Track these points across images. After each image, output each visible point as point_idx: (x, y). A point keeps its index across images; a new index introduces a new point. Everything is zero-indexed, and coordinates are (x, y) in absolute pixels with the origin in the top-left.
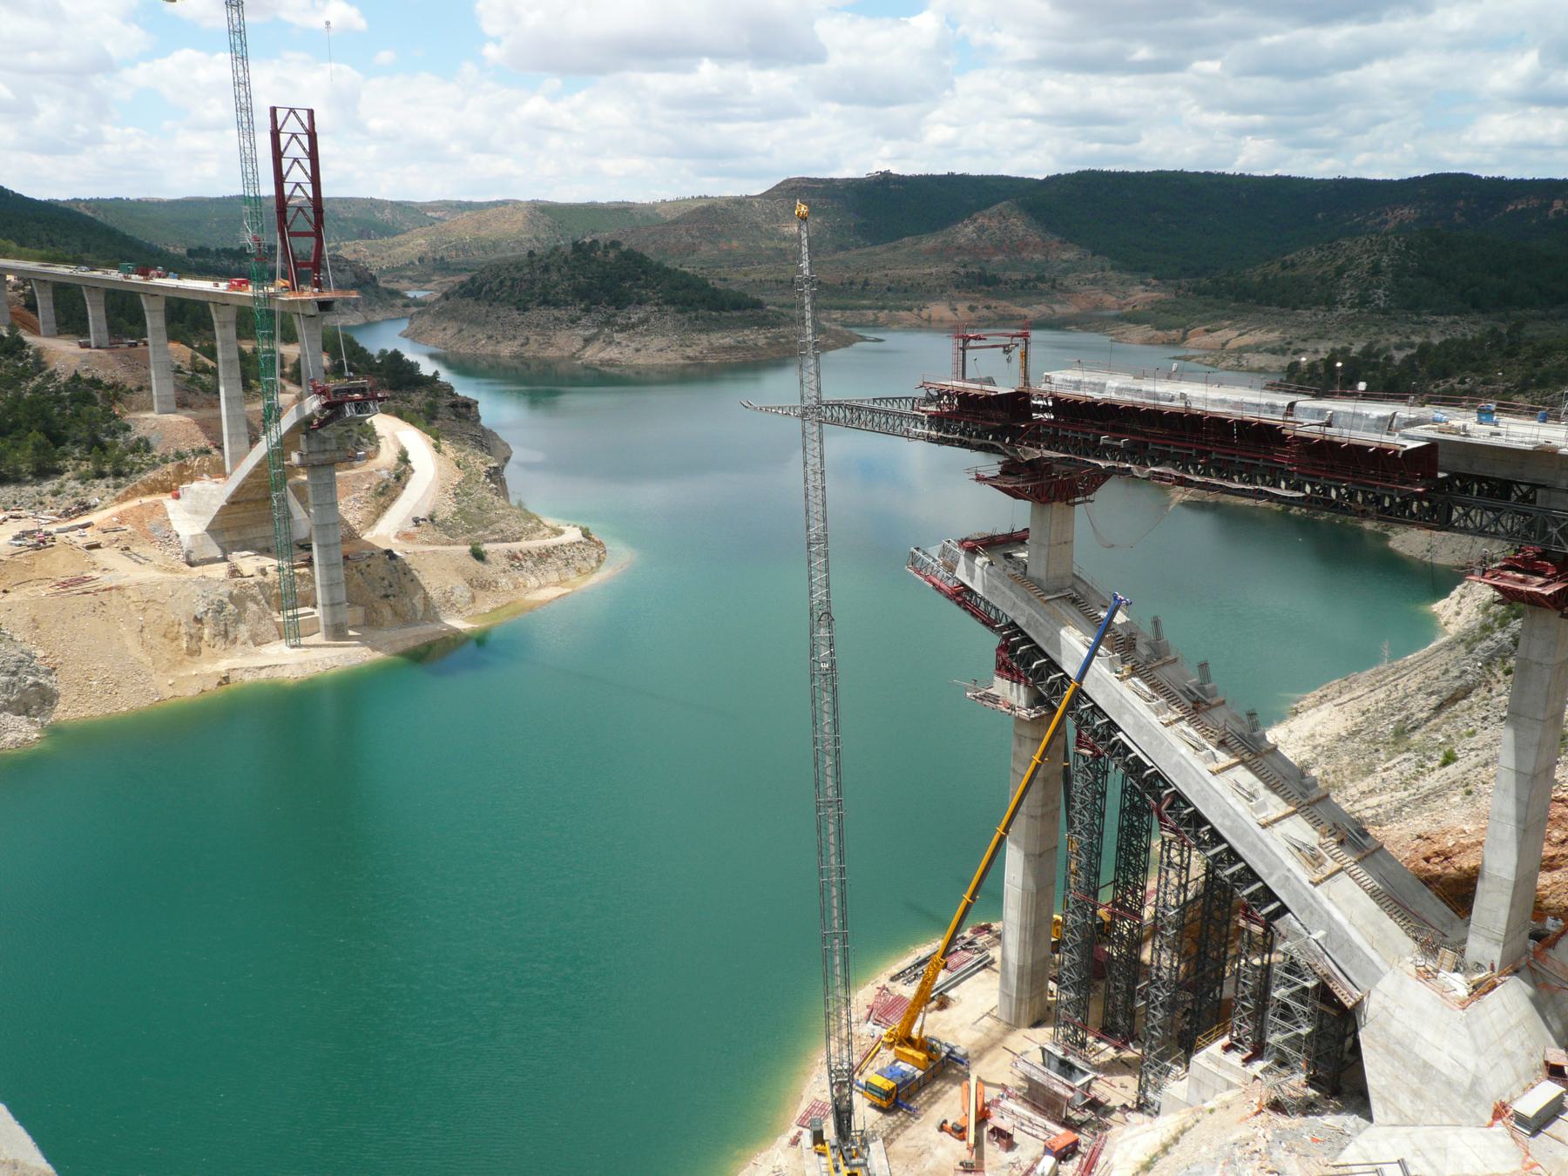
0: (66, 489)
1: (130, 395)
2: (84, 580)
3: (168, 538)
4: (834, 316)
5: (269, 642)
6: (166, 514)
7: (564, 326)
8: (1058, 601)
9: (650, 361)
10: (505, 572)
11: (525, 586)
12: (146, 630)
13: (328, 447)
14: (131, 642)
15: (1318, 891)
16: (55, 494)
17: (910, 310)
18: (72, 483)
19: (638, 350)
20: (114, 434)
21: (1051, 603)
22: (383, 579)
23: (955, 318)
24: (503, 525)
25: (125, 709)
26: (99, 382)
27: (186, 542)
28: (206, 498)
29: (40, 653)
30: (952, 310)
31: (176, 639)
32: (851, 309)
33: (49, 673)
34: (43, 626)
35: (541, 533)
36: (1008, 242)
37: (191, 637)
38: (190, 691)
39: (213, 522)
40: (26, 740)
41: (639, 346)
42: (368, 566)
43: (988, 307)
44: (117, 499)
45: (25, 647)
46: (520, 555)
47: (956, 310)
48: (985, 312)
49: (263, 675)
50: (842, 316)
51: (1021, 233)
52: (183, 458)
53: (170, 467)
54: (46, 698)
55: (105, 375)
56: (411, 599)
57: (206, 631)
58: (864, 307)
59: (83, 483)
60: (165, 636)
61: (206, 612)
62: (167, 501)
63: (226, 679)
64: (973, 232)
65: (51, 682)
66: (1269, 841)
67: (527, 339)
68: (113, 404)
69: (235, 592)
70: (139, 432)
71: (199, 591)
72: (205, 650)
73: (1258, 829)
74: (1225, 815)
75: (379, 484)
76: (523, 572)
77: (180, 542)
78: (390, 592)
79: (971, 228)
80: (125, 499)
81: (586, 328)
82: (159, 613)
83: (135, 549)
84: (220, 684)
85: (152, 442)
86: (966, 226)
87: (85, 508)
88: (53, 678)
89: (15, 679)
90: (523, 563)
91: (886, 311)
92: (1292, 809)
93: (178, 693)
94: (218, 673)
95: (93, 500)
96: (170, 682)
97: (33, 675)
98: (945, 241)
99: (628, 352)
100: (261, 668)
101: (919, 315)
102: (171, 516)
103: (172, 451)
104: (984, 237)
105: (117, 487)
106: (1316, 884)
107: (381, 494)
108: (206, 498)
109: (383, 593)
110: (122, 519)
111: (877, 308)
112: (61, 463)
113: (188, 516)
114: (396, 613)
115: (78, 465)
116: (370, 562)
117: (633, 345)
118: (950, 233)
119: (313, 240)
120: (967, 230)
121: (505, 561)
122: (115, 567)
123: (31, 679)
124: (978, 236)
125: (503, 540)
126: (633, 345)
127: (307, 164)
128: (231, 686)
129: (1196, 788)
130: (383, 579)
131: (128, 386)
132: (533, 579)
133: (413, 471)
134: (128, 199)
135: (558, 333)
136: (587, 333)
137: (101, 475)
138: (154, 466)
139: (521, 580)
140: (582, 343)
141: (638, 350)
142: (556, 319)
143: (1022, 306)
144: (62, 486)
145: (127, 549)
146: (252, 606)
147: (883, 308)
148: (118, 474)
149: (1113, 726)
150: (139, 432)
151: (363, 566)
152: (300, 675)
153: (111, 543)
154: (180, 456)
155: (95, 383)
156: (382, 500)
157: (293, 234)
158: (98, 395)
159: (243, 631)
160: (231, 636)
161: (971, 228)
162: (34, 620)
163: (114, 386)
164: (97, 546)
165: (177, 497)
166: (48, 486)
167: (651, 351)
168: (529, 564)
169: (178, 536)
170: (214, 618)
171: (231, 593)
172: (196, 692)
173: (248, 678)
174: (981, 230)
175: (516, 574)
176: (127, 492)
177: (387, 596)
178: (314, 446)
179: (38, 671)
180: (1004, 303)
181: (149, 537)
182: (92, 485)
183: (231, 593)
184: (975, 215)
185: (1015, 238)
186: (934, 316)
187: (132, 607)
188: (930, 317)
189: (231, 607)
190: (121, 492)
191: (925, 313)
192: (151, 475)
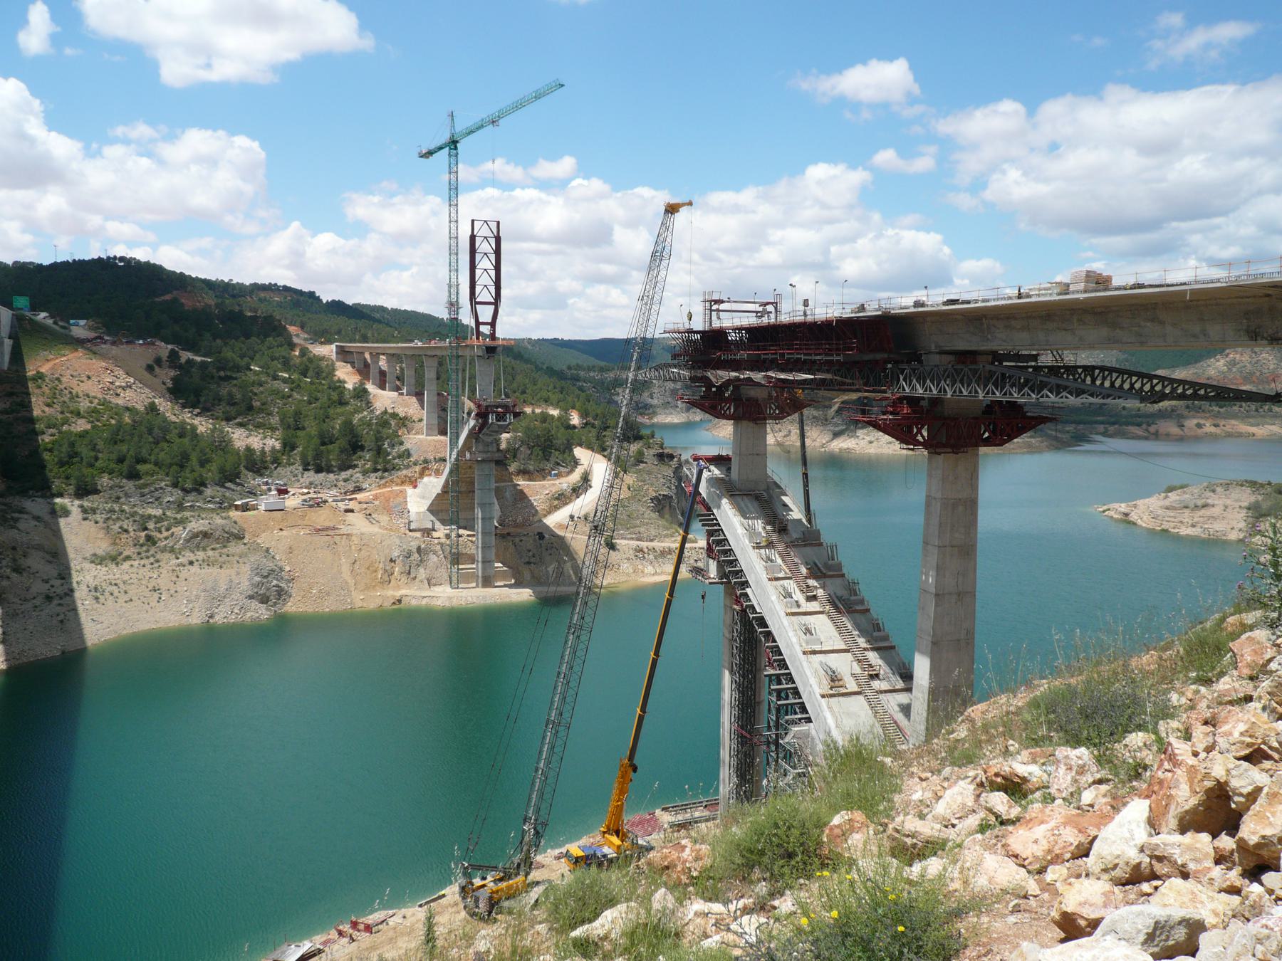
0: (353, 479)
1: (413, 424)
2: (334, 528)
3: (403, 511)
4: (1067, 429)
5: (441, 584)
6: (405, 498)
7: (820, 423)
8: (745, 497)
9: (879, 451)
10: (628, 559)
11: (642, 572)
12: (358, 563)
13: (490, 449)
14: (346, 570)
15: (824, 702)
16: (346, 480)
17: (1139, 425)
18: (358, 475)
19: (871, 442)
20: (393, 446)
21: (737, 497)
22: (529, 551)
23: (1181, 433)
24: (642, 529)
25: (328, 610)
26: (398, 415)
27: (413, 516)
28: (430, 487)
29: (287, 568)
30: (1179, 426)
31: (376, 571)
32: (1085, 423)
33: (289, 581)
34: (295, 552)
35: (673, 539)
36: (1258, 374)
37: (386, 571)
38: (372, 605)
39: (432, 504)
40: (258, 618)
41: (873, 439)
42: (521, 541)
43: (1216, 426)
44: (379, 486)
45: (279, 563)
46: (646, 550)
47: (1183, 426)
48: (1213, 429)
49: (424, 602)
50: (1075, 429)
51: (1272, 367)
52: (427, 463)
53: (418, 468)
54: (281, 593)
55: (401, 412)
56: (546, 568)
57: (397, 569)
58: (1097, 422)
59: (363, 475)
60: (368, 568)
61: (399, 556)
62: (410, 491)
63: (400, 601)
64: (1224, 365)
65: (288, 587)
66: (805, 664)
67: (790, 432)
68: (400, 428)
69: (423, 546)
70: (407, 445)
71: (398, 542)
72: (393, 582)
73: (800, 654)
74: (788, 646)
75: (556, 492)
76: (644, 562)
77: (409, 516)
78: (532, 560)
79: (1222, 362)
80: (385, 486)
81: (836, 425)
82: (368, 553)
83: (373, 516)
84: (394, 603)
85: (412, 452)
86: (1218, 361)
87: (359, 489)
88: (291, 585)
89: (265, 580)
90: (646, 555)
91: (1116, 426)
92: (843, 647)
93: (365, 605)
94: (395, 596)
95: (365, 485)
96: (362, 597)
97: (277, 580)
98: (1196, 373)
99: (863, 443)
100: (424, 597)
101: (1147, 430)
102: (408, 500)
103: (422, 458)
104: (1234, 370)
105: (382, 478)
106: (823, 696)
107: (557, 499)
108: (430, 487)
109: (527, 560)
110: (376, 497)
111: (1108, 423)
112: (356, 462)
113: (419, 499)
114: (533, 576)
115: (365, 464)
116: (524, 538)
117: (868, 438)
118: (1202, 366)
119: (493, 307)
120: (1218, 363)
121: (631, 552)
122: (357, 523)
123: (275, 582)
124: (1229, 369)
125: (638, 539)
126: (868, 438)
127: (493, 257)
128: (401, 605)
129: (777, 626)
130: (529, 551)
131: (414, 418)
132: (650, 567)
133: (591, 487)
134: (562, 339)
135: (814, 428)
136: (837, 429)
137: (376, 470)
138: (408, 467)
139: (640, 567)
140: (831, 436)
141: (871, 442)
142: (814, 417)
143: (1252, 425)
144: (352, 476)
145: (370, 515)
146: (433, 558)
147: (1114, 423)
148: (385, 470)
149: (745, 584)
150: (407, 445)
151: (517, 540)
152: (447, 605)
153: (361, 510)
154: (426, 461)
155: (395, 415)
156: (556, 503)
157: (476, 303)
158: (393, 423)
159: (422, 573)
160: (412, 575)
161: (1222, 362)
162: (290, 548)
163: (406, 418)
164: (352, 511)
165: (415, 487)
166: (344, 475)
167: (881, 443)
168: (651, 557)
169: (409, 512)
170: (403, 561)
171: (419, 547)
172: (376, 606)
173: (414, 602)
174: (1233, 363)
175: (638, 562)
176: (387, 482)
177: (529, 563)
178: (481, 447)
179: (282, 578)
180: (1233, 422)
181: (388, 510)
182: (369, 477)
183: (419, 547)
184: (1227, 351)
185: (1266, 371)
186: (1162, 431)
187: (353, 547)
188: (1157, 431)
189: (416, 555)
190: (383, 481)
191: (1152, 429)
192: (404, 472)
